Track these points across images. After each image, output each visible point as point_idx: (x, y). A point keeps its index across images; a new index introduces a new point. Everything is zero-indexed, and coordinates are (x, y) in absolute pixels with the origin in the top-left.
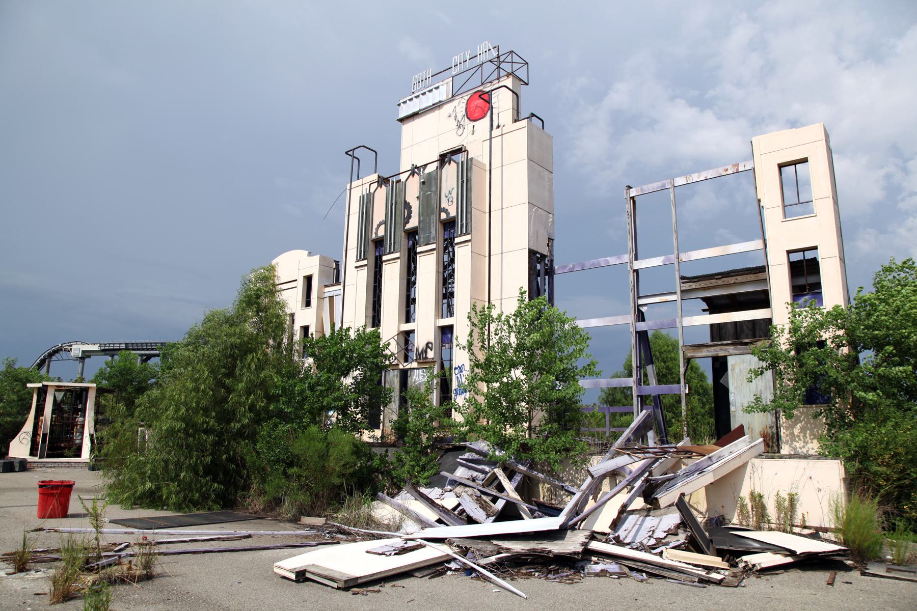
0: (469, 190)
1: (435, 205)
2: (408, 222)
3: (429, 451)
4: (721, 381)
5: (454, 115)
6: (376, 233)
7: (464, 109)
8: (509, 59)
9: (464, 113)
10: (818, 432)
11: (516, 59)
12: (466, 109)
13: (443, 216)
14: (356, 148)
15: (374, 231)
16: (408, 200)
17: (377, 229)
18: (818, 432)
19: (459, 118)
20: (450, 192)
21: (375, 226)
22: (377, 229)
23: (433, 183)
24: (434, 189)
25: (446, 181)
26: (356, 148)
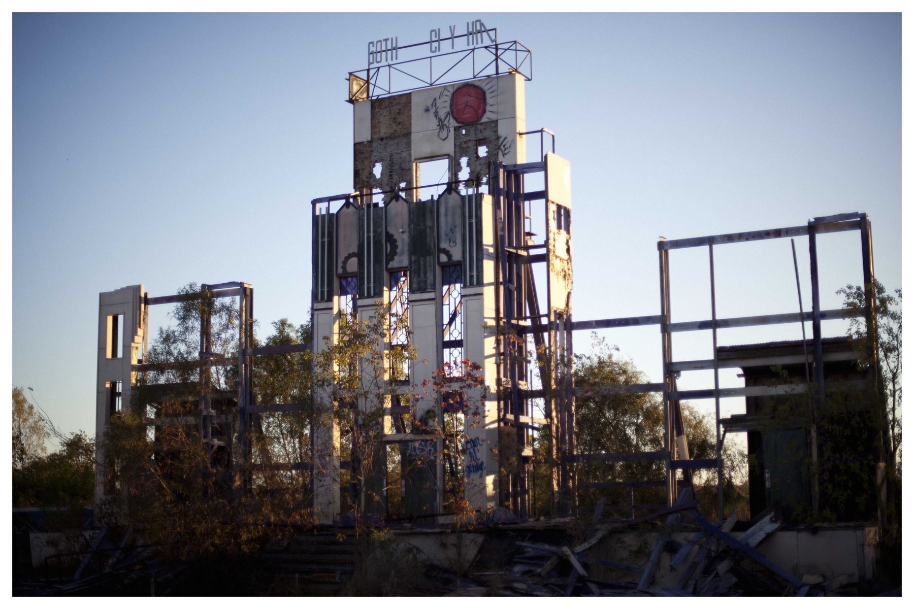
0: (661, 267)
1: (432, 244)
2: (392, 259)
3: (613, 437)
4: (542, 389)
5: (434, 109)
6: (344, 267)
7: (448, 104)
8: (513, 47)
9: (448, 109)
10: (296, 427)
11: (519, 47)
12: (451, 106)
13: (444, 258)
14: (730, 238)
15: (340, 265)
16: (391, 231)
17: (345, 263)
18: (296, 427)
19: (442, 114)
20: (451, 229)
21: (341, 259)
22: (345, 263)
23: (428, 216)
24: (429, 223)
25: (446, 215)
26: (730, 238)
